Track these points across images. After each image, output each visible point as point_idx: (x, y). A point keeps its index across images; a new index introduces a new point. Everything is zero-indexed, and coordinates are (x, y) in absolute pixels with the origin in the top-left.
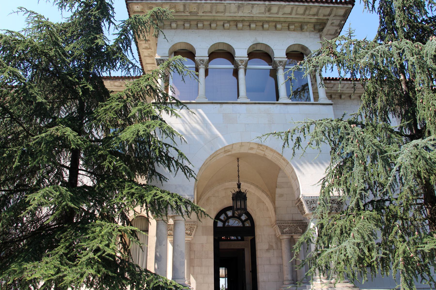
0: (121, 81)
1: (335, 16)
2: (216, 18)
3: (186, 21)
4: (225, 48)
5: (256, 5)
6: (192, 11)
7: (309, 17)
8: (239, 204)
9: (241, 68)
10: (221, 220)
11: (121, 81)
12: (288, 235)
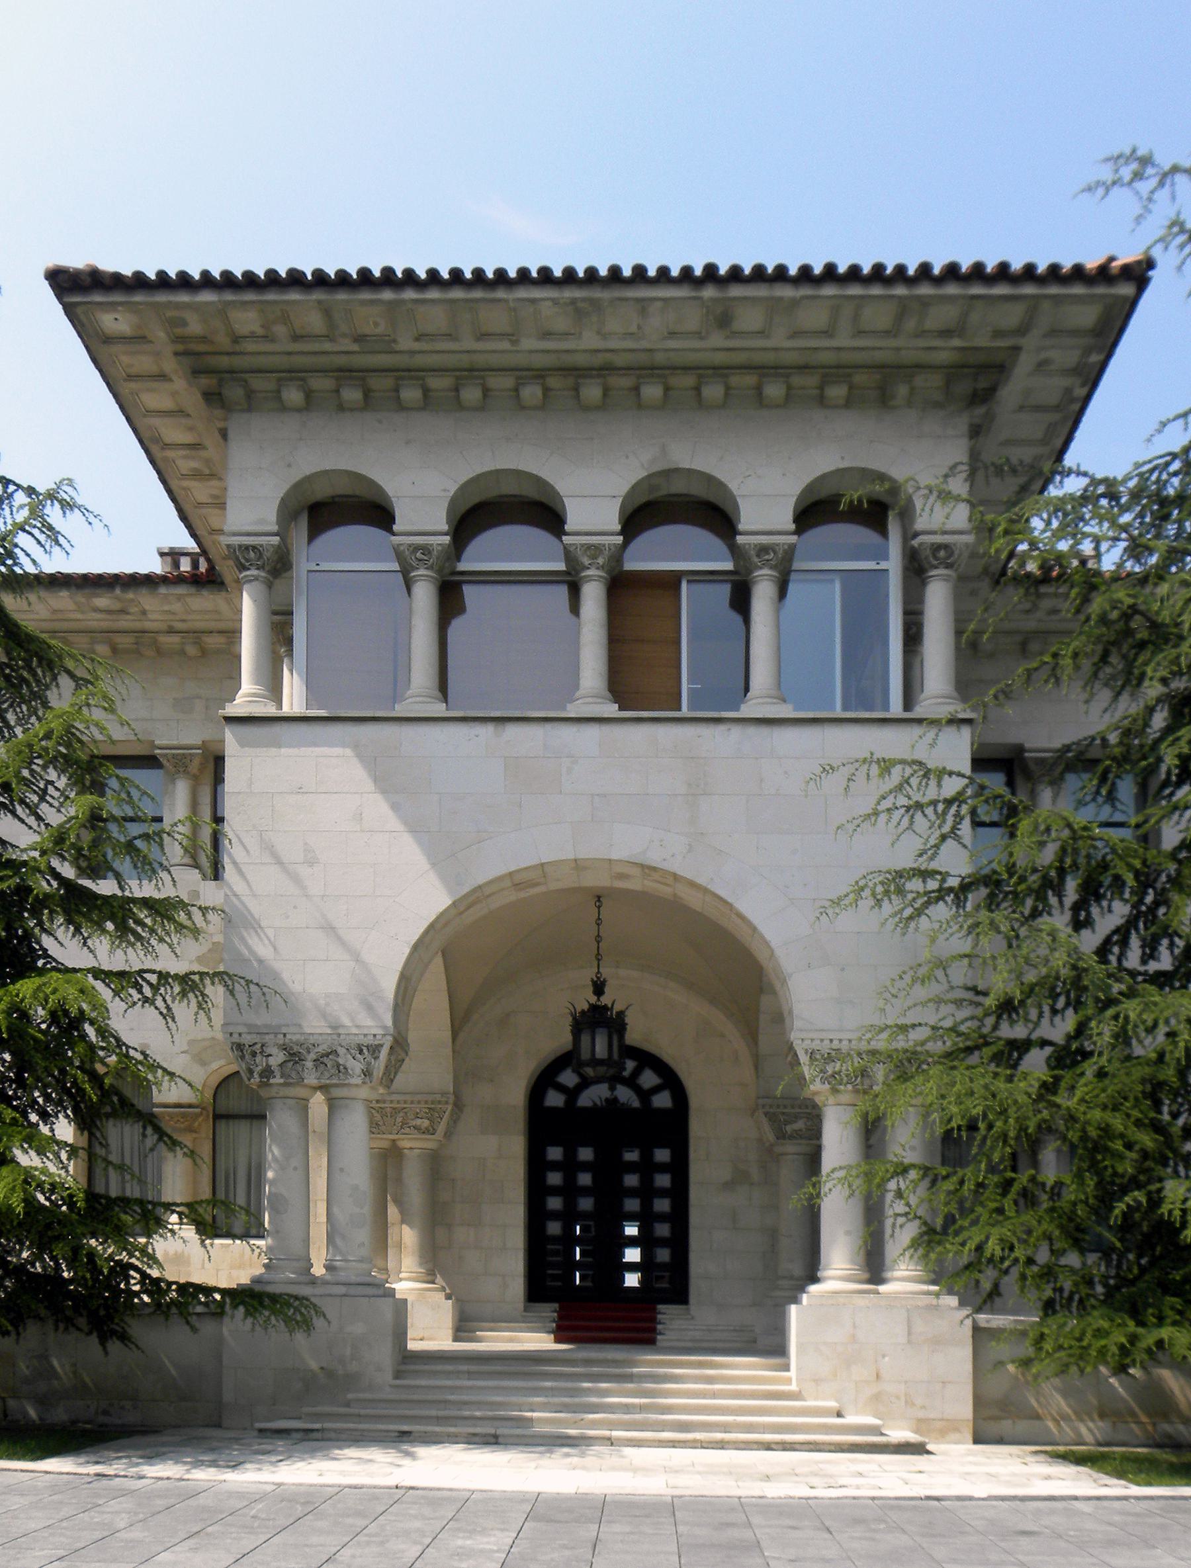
0: (118, 591)
1: (1053, 332)
2: (481, 360)
3: (345, 374)
4: (531, 492)
5: (659, 304)
6: (367, 331)
7: (922, 343)
8: (598, 1048)
9: (589, 579)
11: (118, 591)
12: (803, 1141)
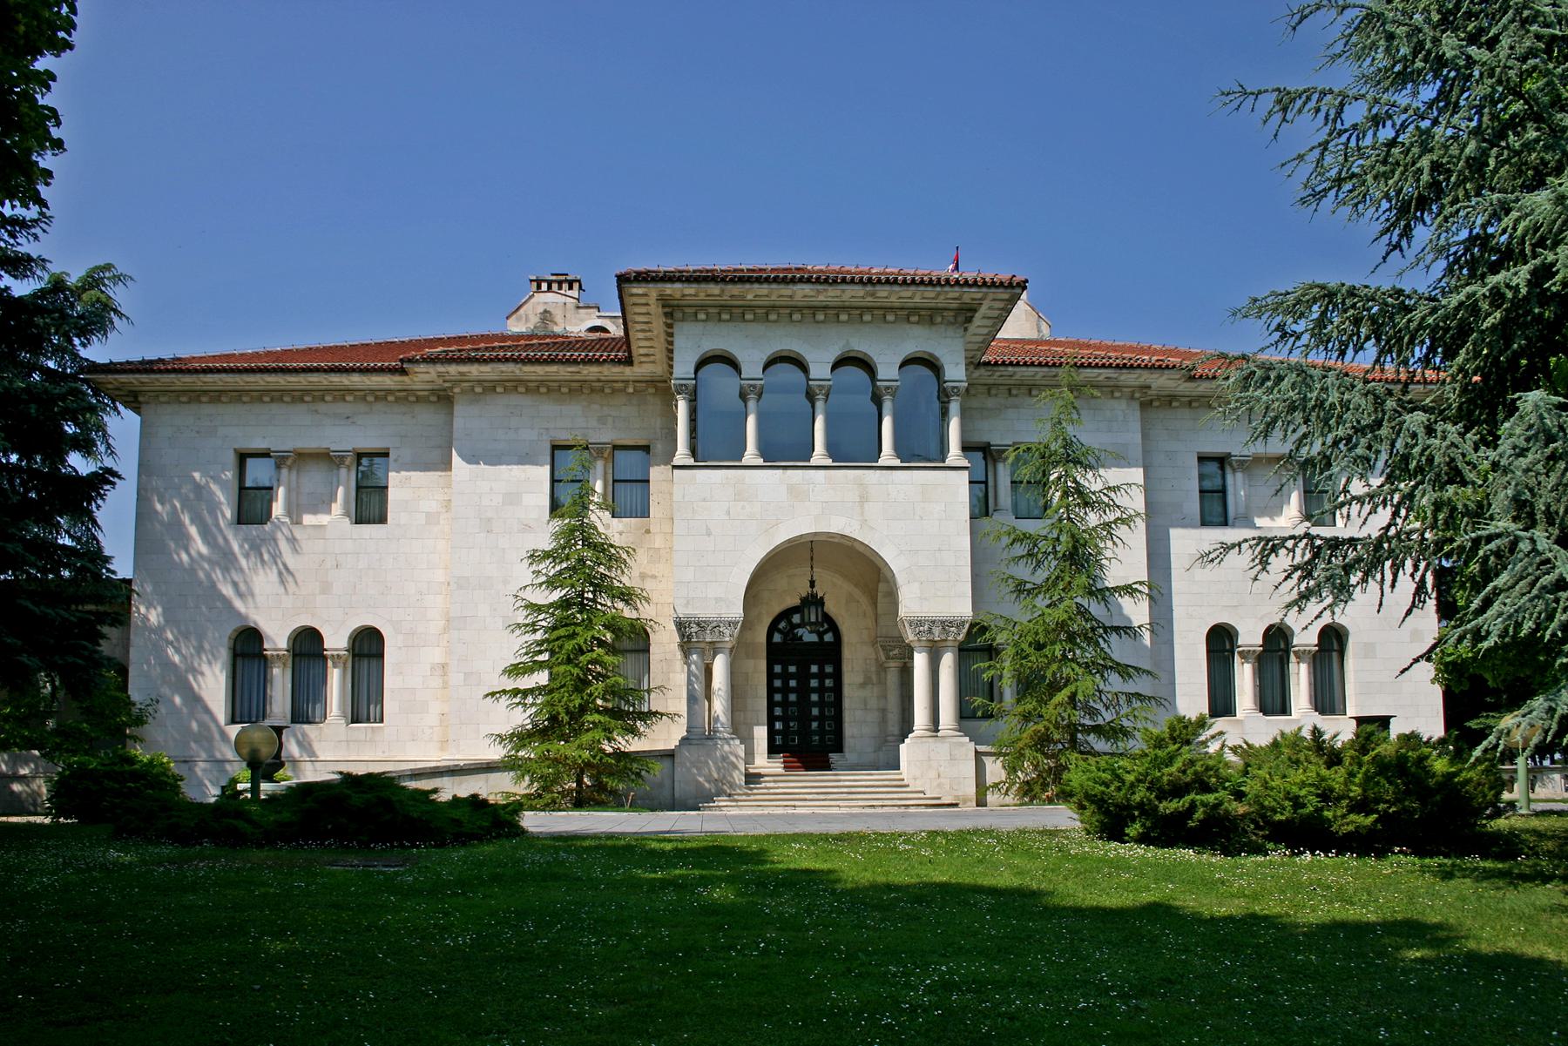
10: (780, 631)
